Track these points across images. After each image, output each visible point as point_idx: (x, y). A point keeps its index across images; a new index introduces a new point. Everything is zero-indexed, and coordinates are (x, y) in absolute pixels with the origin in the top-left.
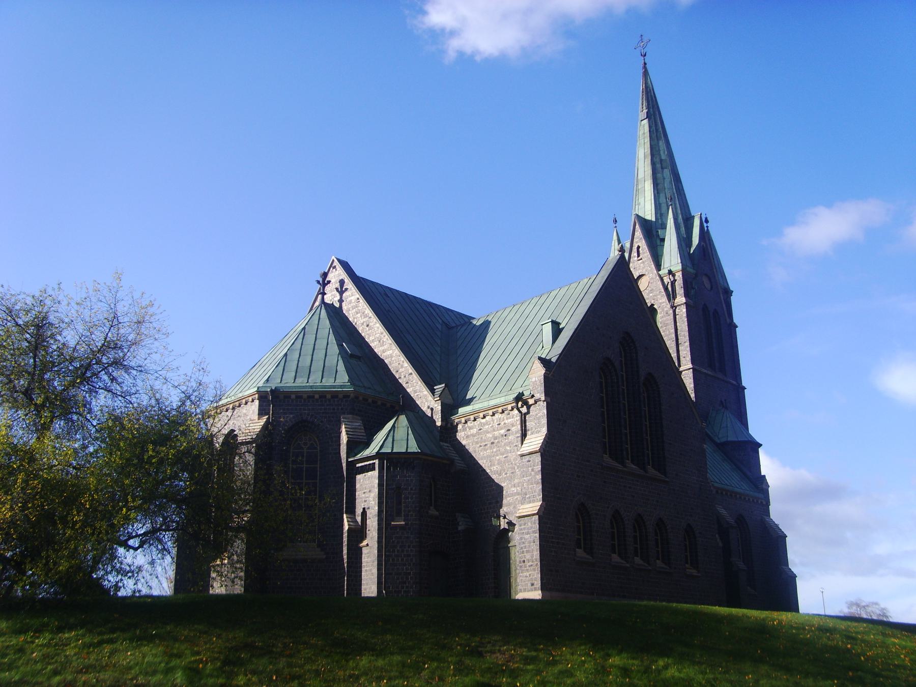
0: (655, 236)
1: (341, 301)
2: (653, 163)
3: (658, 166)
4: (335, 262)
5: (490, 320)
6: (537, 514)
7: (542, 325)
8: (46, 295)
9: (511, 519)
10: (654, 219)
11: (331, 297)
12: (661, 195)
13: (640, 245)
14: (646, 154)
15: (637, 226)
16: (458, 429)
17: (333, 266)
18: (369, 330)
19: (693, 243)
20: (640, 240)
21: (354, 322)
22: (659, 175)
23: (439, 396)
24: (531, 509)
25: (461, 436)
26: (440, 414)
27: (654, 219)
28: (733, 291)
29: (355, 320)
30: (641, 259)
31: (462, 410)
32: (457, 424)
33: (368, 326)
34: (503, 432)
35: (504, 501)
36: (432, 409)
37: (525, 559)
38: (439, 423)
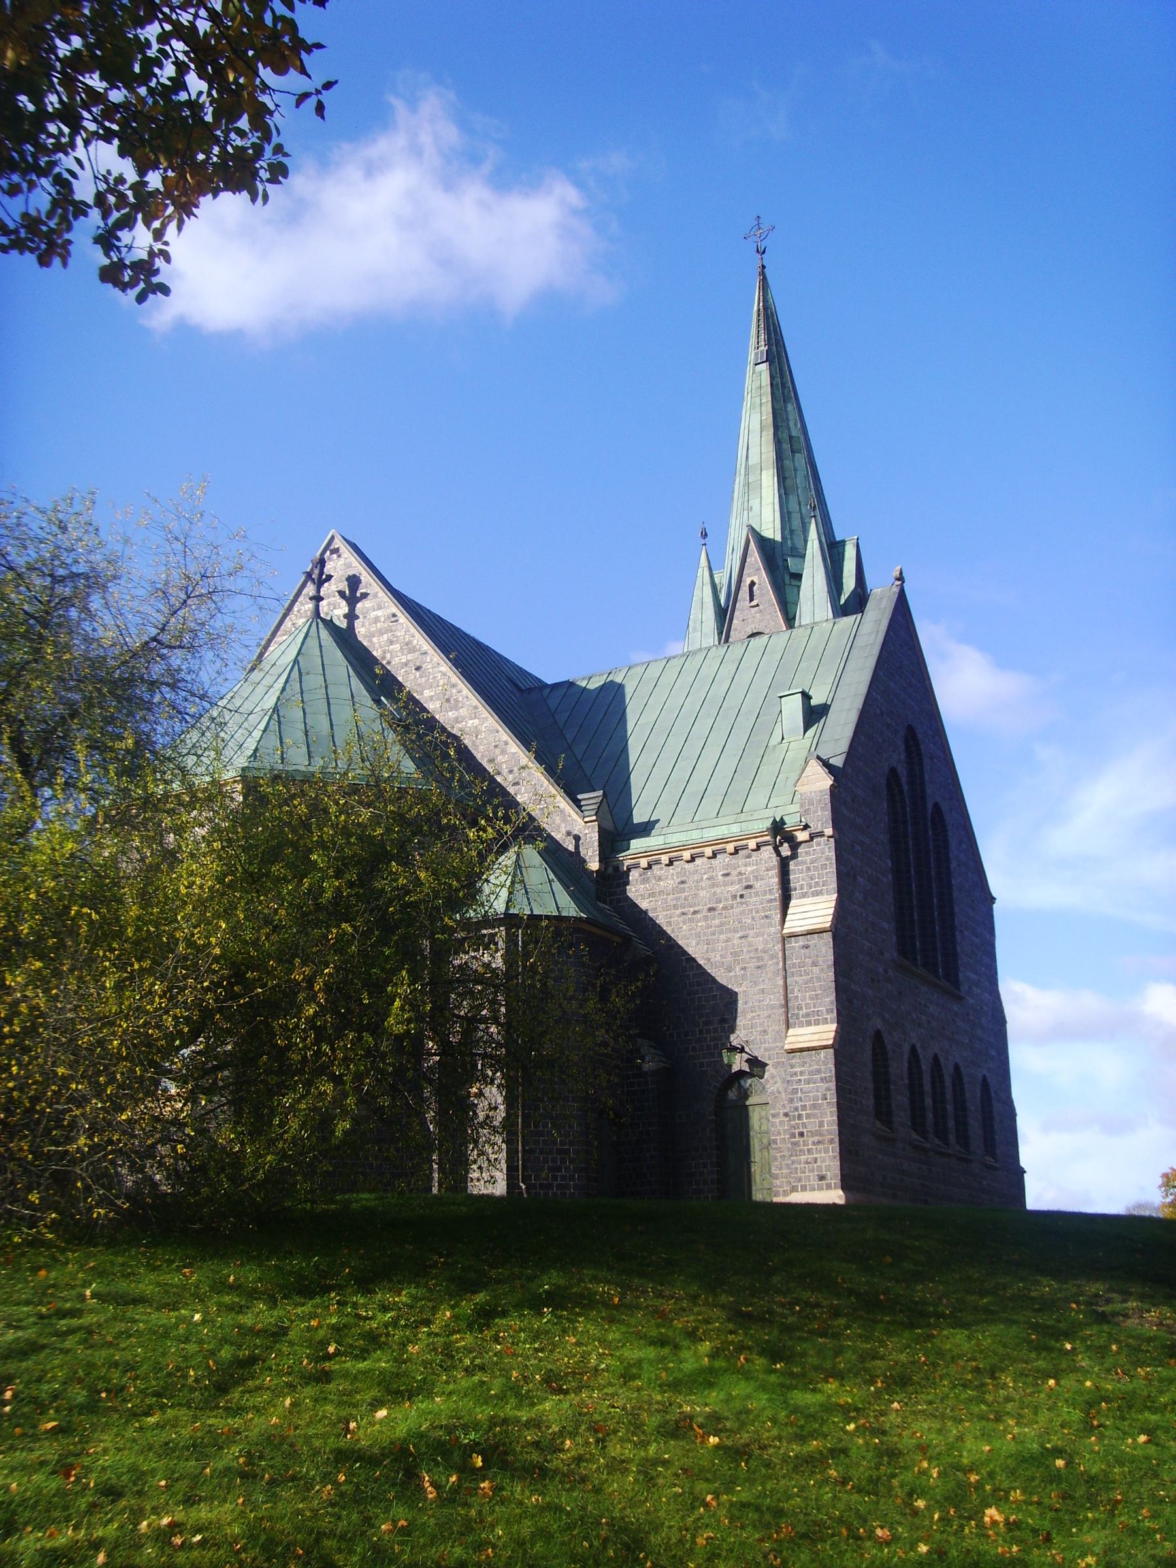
0: (782, 568)
1: (351, 617)
2: (778, 442)
3: (786, 446)
4: (336, 540)
5: (618, 680)
6: (832, 1046)
7: (781, 697)
8: (71, 510)
9: (756, 1054)
10: (778, 538)
11: (335, 610)
12: (791, 497)
13: (756, 580)
14: (764, 423)
15: (752, 544)
16: (631, 878)
17: (331, 548)
18: (421, 677)
19: (844, 586)
20: (757, 574)
21: (384, 658)
22: (787, 463)
23: (596, 815)
24: (816, 1037)
25: (638, 891)
26: (597, 848)
27: (778, 538)
28: (613, 694)
29: (388, 656)
30: (758, 605)
31: (637, 845)
32: (629, 870)
33: (418, 669)
34: (736, 888)
35: (738, 1019)
36: (577, 838)
37: (805, 1130)
38: (594, 865)
